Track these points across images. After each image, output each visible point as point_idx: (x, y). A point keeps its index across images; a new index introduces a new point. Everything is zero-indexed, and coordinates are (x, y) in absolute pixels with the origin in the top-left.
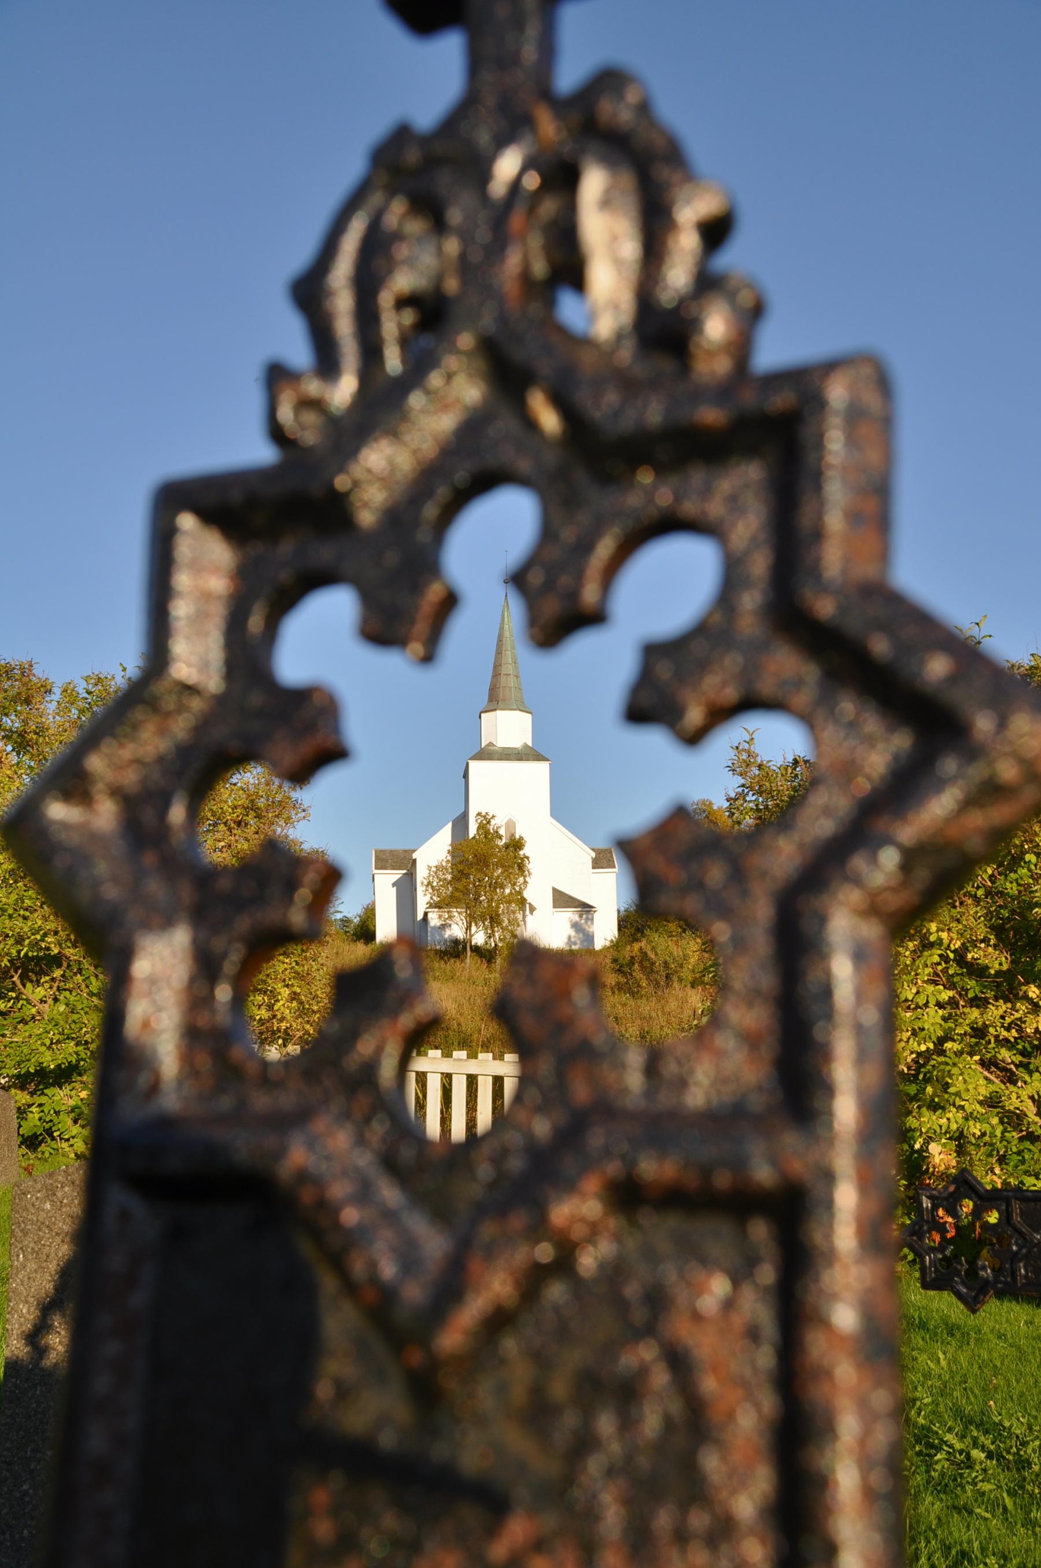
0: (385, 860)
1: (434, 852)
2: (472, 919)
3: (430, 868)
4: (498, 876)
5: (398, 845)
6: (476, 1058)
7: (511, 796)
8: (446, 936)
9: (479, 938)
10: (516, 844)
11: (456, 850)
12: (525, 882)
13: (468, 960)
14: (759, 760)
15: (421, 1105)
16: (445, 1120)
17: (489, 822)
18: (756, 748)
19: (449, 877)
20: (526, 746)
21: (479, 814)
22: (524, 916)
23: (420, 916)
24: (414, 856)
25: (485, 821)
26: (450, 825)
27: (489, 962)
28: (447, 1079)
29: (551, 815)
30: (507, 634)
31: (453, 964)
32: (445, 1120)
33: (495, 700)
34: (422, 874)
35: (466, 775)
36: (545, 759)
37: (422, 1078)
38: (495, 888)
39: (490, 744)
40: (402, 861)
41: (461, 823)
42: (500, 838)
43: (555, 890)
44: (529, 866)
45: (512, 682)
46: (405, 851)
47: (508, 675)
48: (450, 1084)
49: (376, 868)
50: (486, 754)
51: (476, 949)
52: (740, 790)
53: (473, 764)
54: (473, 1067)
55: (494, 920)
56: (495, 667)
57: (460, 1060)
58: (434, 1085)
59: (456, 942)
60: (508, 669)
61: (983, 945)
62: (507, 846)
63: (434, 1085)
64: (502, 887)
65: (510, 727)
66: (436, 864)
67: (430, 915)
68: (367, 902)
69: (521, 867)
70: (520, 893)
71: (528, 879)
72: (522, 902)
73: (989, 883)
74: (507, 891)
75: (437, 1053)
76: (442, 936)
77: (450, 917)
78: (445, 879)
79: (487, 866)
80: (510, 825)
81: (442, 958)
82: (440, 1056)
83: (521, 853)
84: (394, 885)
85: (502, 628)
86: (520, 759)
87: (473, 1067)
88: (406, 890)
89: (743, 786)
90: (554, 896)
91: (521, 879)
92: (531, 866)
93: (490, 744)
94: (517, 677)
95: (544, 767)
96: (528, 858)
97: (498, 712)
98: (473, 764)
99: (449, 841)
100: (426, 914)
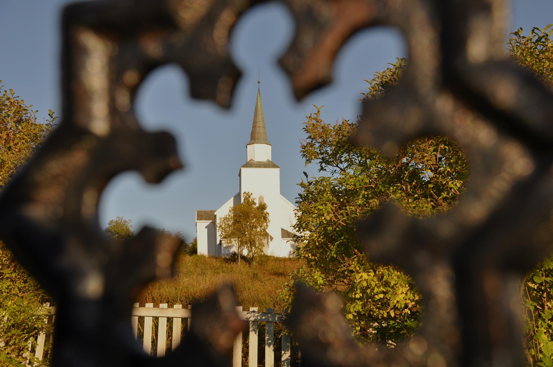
0: (202, 216)
1: (224, 211)
2: (242, 244)
3: (220, 219)
4: (254, 223)
5: (208, 209)
6: (144, 306)
7: (265, 186)
8: (231, 251)
9: (245, 252)
10: (263, 207)
11: (234, 209)
12: (267, 225)
13: (239, 263)
14: (322, 124)
15: (141, 335)
16: (155, 342)
17: (249, 197)
18: (321, 117)
19: (230, 223)
20: (268, 161)
21: (245, 193)
22: (268, 242)
23: (218, 242)
24: (215, 213)
25: (248, 195)
26: (233, 198)
27: (249, 264)
28: (156, 319)
29: (281, 193)
30: (259, 107)
31: (234, 265)
32: (155, 342)
33: (254, 139)
34: (218, 221)
35: (240, 175)
36: (277, 167)
37: (141, 319)
38: (253, 228)
39: (252, 160)
40: (210, 216)
41: (238, 197)
42: (255, 204)
43: (282, 229)
44: (269, 218)
45: (262, 130)
46: (212, 211)
47: (260, 127)
48: (158, 324)
49: (197, 220)
50: (249, 165)
51: (244, 258)
52: (309, 140)
53: (243, 170)
54: (170, 313)
55: (252, 243)
56: (254, 123)
57: (163, 309)
58: (148, 324)
59: (235, 254)
60: (260, 124)
61: (314, 141)
62: (258, 208)
63: (148, 324)
64: (256, 227)
65: (261, 152)
66: (223, 216)
67: (223, 242)
68: (194, 237)
69: (265, 219)
70: (264, 230)
71: (268, 224)
72: (266, 235)
73: (458, 193)
74: (258, 230)
75: (151, 305)
76: (229, 251)
77: (231, 242)
78: (228, 224)
79: (249, 217)
80: (261, 198)
81: (227, 262)
82: (152, 306)
83: (265, 211)
84: (206, 227)
85: (257, 105)
86: (266, 167)
87: (170, 313)
88: (212, 230)
89: (310, 137)
90: (282, 232)
91: (265, 224)
92: (270, 217)
93: (252, 160)
94: (264, 128)
95: (277, 170)
96: (268, 214)
97: (255, 145)
98: (243, 170)
99: (232, 205)
100: (221, 241)
